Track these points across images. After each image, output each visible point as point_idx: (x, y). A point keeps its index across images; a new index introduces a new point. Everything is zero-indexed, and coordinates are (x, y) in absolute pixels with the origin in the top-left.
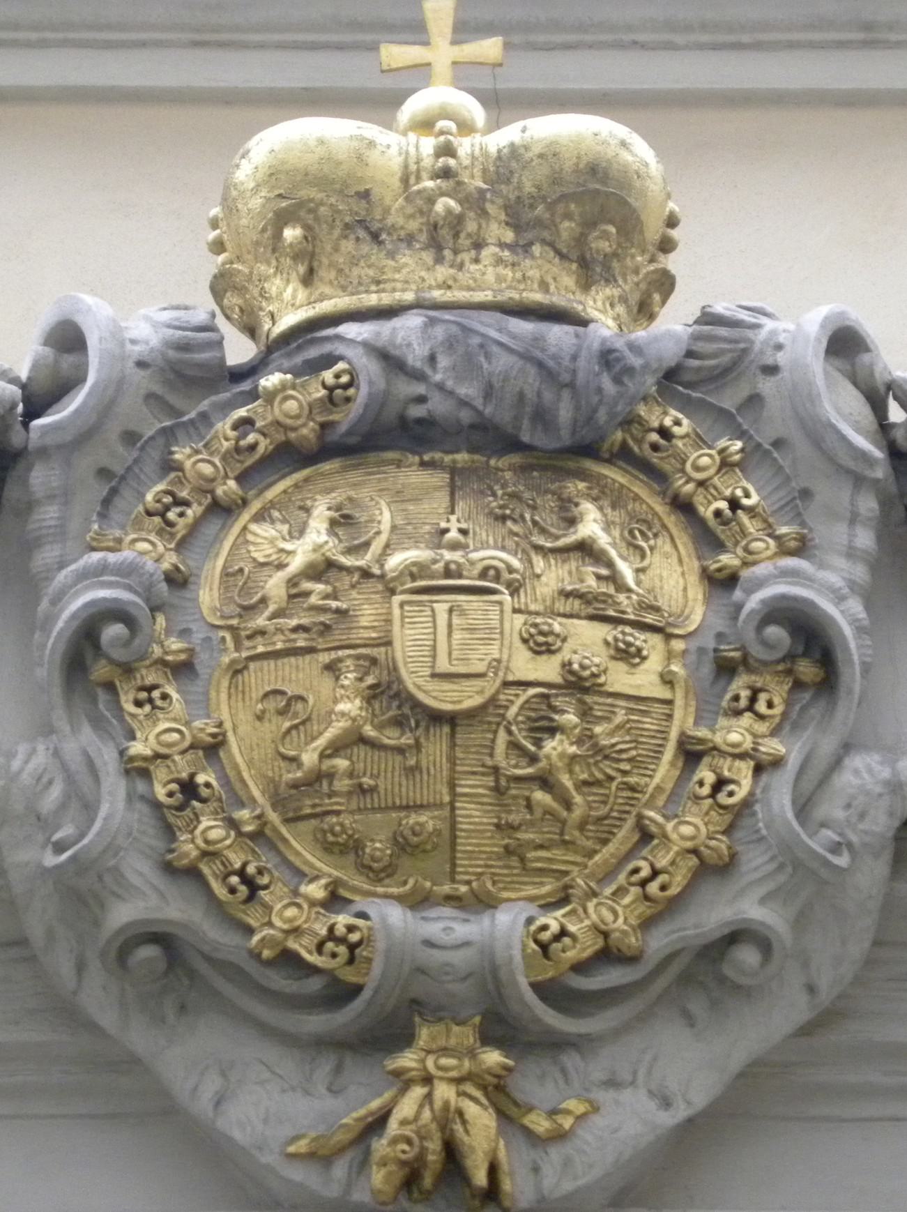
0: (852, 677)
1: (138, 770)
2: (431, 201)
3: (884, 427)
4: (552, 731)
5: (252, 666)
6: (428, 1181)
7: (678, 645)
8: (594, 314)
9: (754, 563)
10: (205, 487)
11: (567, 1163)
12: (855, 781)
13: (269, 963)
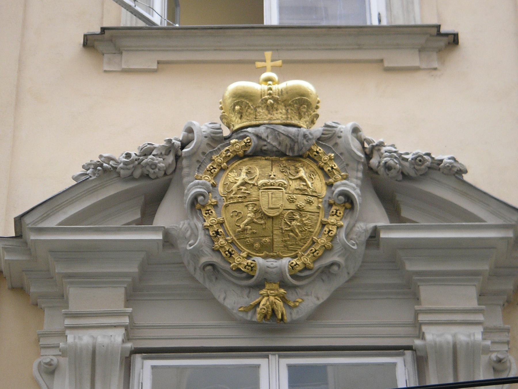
0: (358, 207)
1: (206, 229)
2: (267, 100)
3: (364, 148)
4: (294, 220)
5: (230, 205)
6: (268, 317)
7: (320, 200)
8: (302, 125)
9: (337, 181)
10: (219, 165)
11: (298, 312)
12: (358, 229)
13: (234, 271)
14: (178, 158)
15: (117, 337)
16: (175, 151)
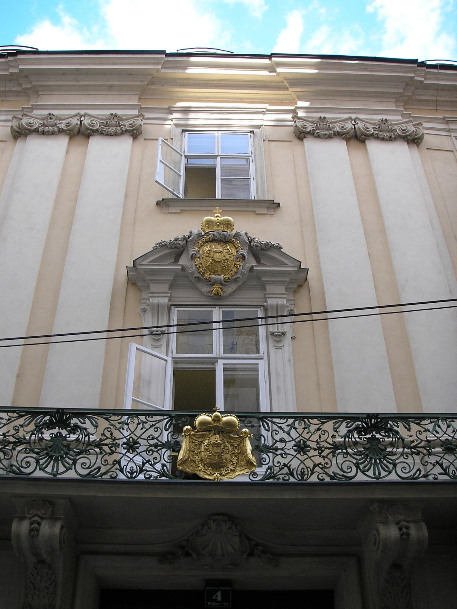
0: (246, 259)
1: (196, 265)
14: (187, 241)
15: (166, 300)
16: (185, 239)
